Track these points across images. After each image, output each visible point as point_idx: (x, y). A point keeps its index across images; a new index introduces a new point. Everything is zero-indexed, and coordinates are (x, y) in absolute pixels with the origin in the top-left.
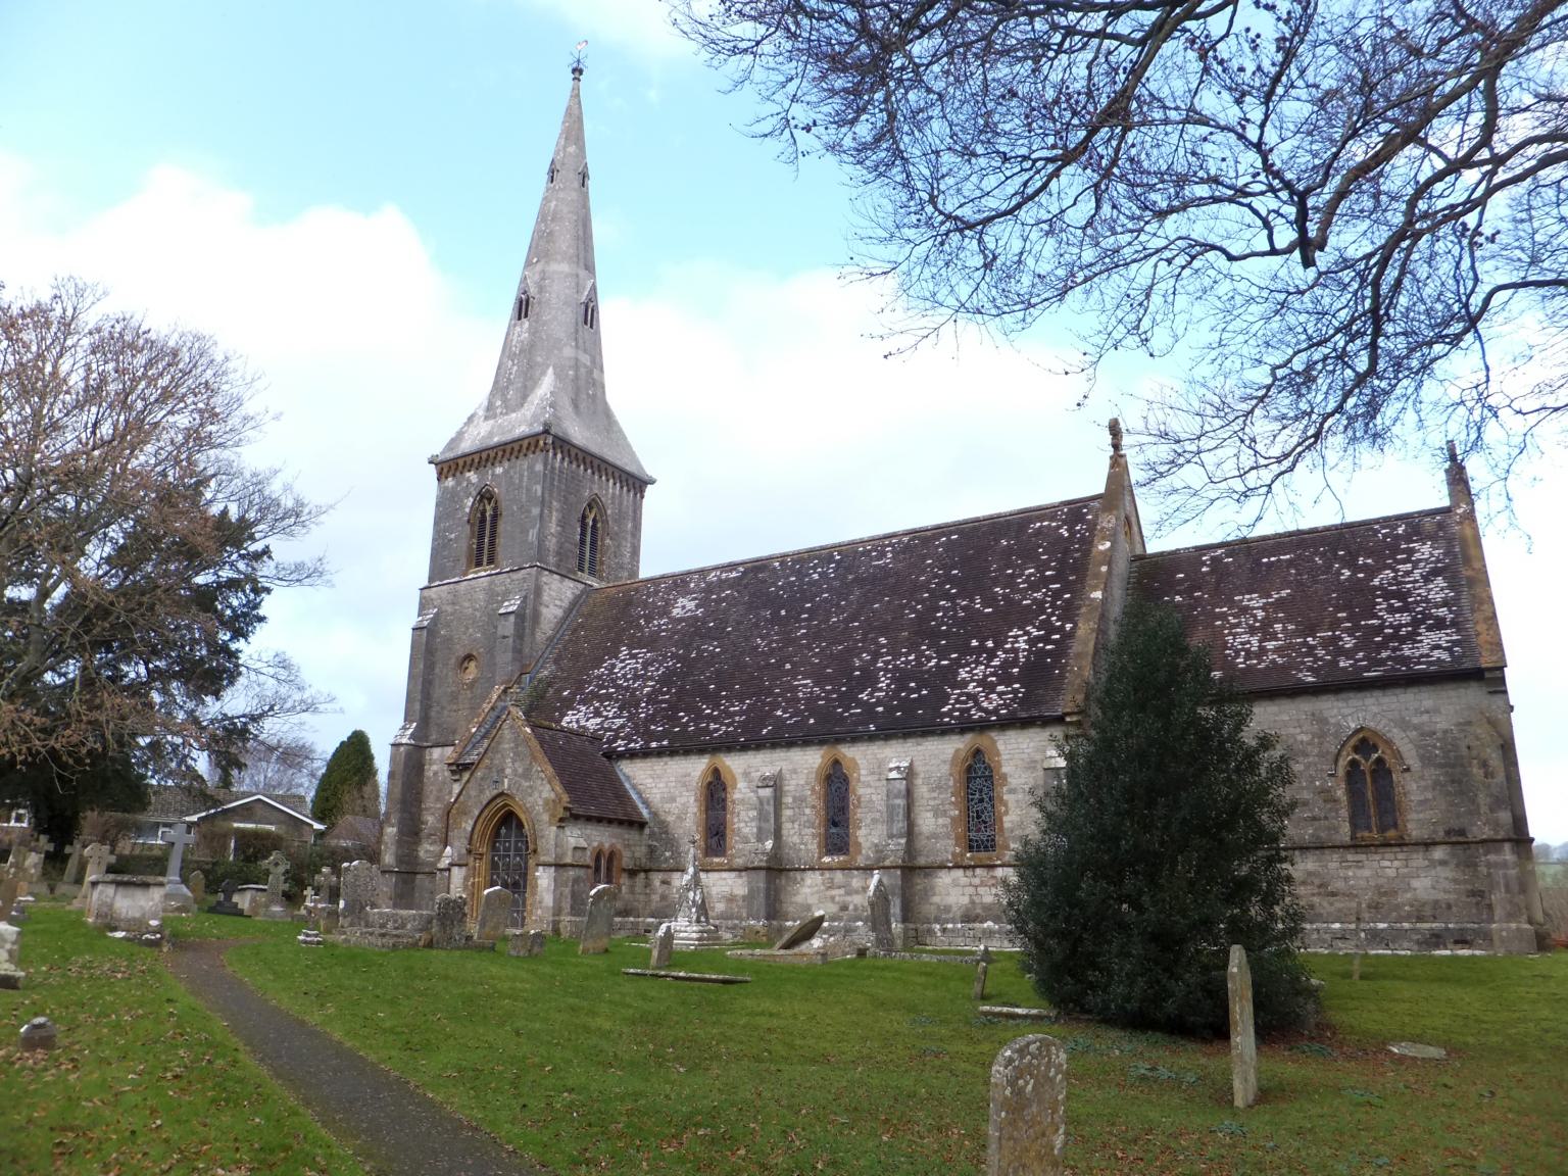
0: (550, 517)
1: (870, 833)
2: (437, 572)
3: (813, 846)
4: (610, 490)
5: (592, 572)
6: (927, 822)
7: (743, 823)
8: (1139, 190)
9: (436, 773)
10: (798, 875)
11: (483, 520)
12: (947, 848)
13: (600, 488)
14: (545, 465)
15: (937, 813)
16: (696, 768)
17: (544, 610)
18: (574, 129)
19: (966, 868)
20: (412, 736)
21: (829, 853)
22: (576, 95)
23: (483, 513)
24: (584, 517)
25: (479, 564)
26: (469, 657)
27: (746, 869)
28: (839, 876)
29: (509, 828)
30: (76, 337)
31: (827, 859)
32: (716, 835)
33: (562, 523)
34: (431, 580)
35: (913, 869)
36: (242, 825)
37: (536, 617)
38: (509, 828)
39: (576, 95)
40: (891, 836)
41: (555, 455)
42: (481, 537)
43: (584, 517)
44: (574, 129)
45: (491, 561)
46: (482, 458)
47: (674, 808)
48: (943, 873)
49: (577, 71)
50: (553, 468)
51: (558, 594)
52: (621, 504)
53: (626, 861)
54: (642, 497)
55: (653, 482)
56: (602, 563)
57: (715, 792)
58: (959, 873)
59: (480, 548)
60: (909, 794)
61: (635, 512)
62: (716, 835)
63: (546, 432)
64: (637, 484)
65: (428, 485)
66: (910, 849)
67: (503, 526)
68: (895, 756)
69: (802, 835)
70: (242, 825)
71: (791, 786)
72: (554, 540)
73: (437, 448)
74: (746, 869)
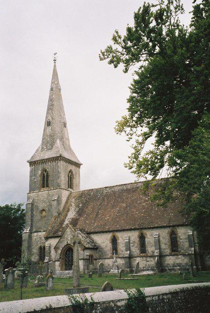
1: (150, 249)
2: (32, 189)
3: (138, 252)
4: (73, 168)
5: (71, 188)
6: (163, 246)
7: (121, 247)
9: (35, 239)
10: (135, 258)
11: (44, 177)
12: (168, 251)
15: (165, 244)
16: (109, 236)
18: (55, 74)
19: (172, 255)
20: (29, 231)
21: (141, 253)
22: (55, 66)
23: (44, 174)
25: (43, 187)
26: (43, 210)
27: (124, 258)
28: (145, 259)
29: (69, 251)
31: (141, 254)
32: (115, 248)
34: (30, 191)
35: (161, 256)
38: (69, 251)
39: (55, 66)
40: (156, 249)
42: (71, 184)
44: (55, 74)
45: (47, 186)
46: (43, 161)
47: (104, 245)
49: (55, 60)
51: (65, 194)
53: (94, 257)
57: (114, 241)
58: (171, 257)
59: (44, 183)
60: (159, 241)
62: (115, 248)
64: (78, 165)
65: (27, 169)
66: (160, 252)
67: (50, 178)
68: (155, 233)
69: (136, 250)
71: (132, 239)
73: (29, 158)
74: (124, 258)
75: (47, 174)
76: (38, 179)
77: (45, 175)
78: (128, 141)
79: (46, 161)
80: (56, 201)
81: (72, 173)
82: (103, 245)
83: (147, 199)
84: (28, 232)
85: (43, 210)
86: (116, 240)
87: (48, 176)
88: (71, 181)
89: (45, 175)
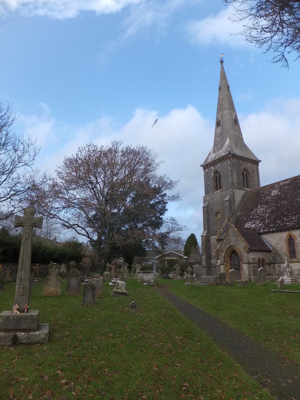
4: (249, 166)
5: (247, 187)
9: (213, 242)
11: (217, 178)
16: (285, 235)
18: (223, 76)
22: (222, 68)
23: (216, 176)
25: (217, 189)
26: (218, 213)
39: (222, 68)
42: (217, 182)
44: (223, 76)
45: (220, 188)
49: (222, 62)
67: (222, 179)
73: (202, 162)
75: (219, 175)
76: (212, 183)
77: (218, 176)
78: (260, 48)
79: (216, 161)
80: (228, 202)
81: (248, 171)
82: (278, 247)
83: (61, 398)
84: (204, 235)
85: (218, 213)
86: (293, 240)
87: (220, 177)
88: (247, 179)
89: (218, 176)
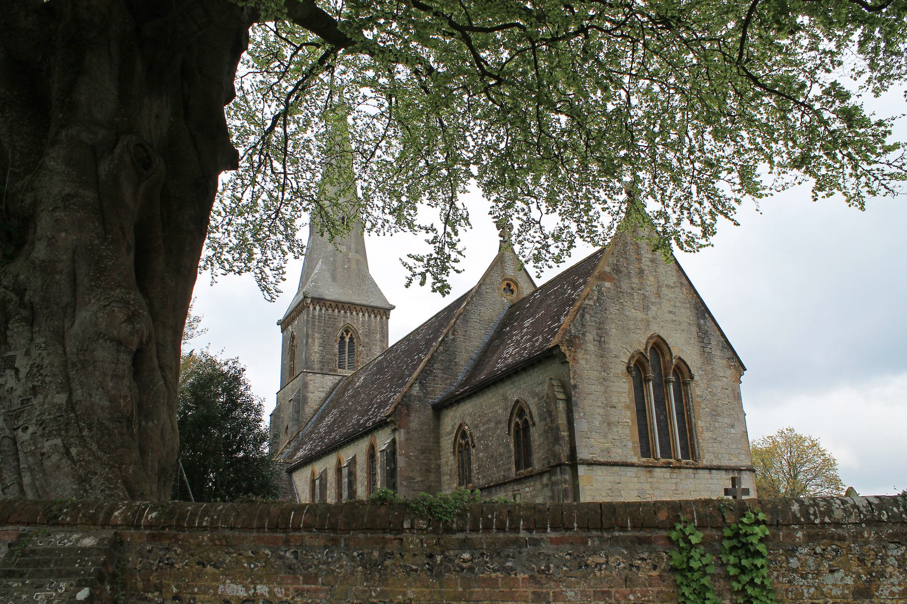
0: (314, 344)
4: (358, 321)
8: (543, 134)
13: (352, 319)
14: (308, 315)
17: (310, 395)
24: (342, 338)
30: (544, 210)
33: (323, 345)
36: (379, 483)
37: (305, 399)
41: (315, 308)
43: (342, 338)
48: (658, 470)
50: (314, 316)
52: (369, 325)
54: (388, 318)
55: (394, 307)
56: (358, 362)
61: (382, 328)
63: (305, 297)
70: (379, 483)
72: (317, 355)
